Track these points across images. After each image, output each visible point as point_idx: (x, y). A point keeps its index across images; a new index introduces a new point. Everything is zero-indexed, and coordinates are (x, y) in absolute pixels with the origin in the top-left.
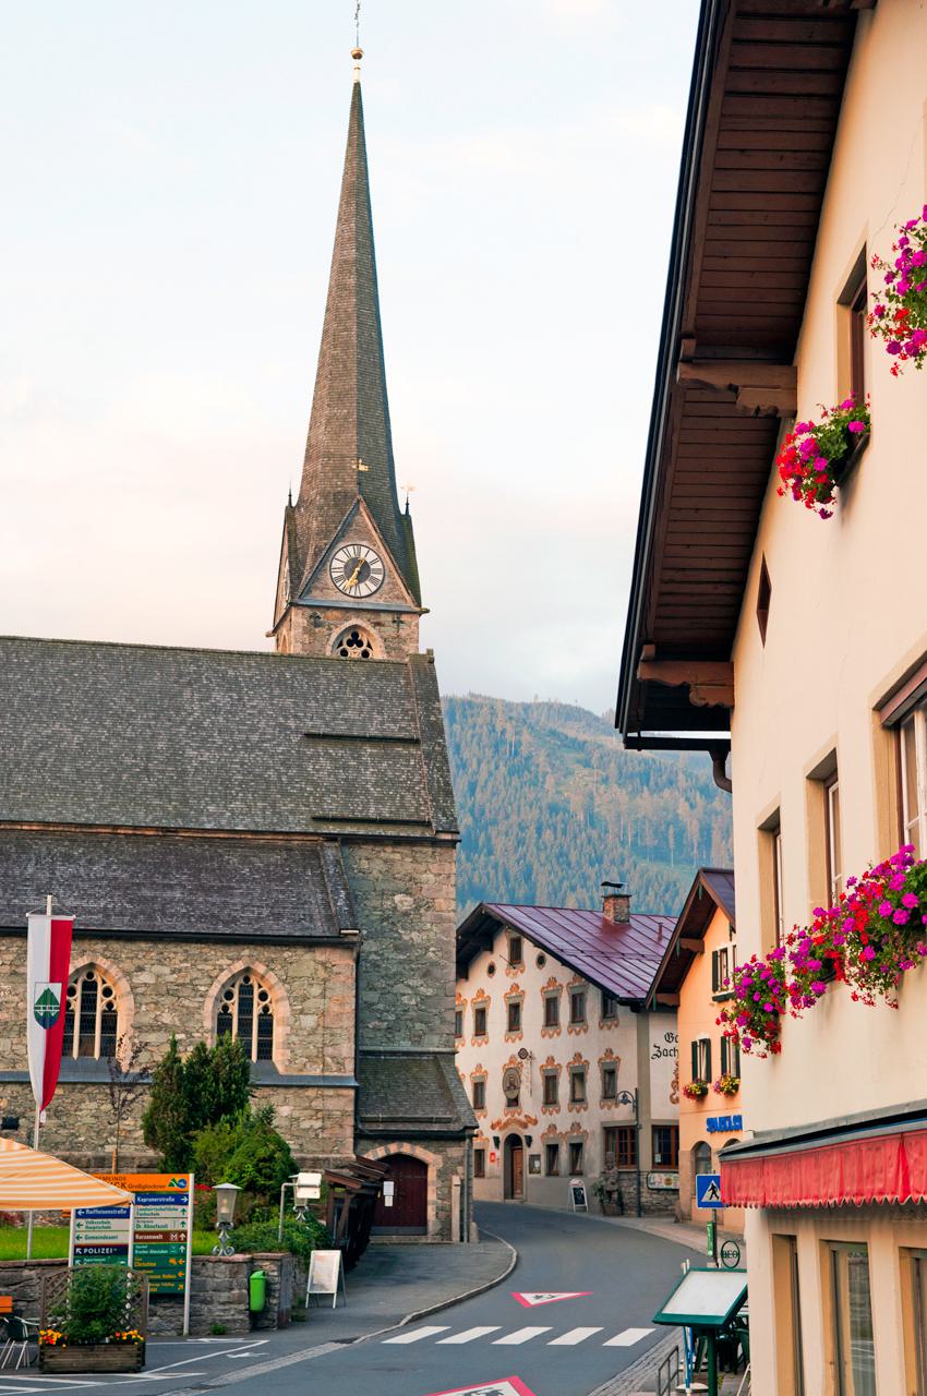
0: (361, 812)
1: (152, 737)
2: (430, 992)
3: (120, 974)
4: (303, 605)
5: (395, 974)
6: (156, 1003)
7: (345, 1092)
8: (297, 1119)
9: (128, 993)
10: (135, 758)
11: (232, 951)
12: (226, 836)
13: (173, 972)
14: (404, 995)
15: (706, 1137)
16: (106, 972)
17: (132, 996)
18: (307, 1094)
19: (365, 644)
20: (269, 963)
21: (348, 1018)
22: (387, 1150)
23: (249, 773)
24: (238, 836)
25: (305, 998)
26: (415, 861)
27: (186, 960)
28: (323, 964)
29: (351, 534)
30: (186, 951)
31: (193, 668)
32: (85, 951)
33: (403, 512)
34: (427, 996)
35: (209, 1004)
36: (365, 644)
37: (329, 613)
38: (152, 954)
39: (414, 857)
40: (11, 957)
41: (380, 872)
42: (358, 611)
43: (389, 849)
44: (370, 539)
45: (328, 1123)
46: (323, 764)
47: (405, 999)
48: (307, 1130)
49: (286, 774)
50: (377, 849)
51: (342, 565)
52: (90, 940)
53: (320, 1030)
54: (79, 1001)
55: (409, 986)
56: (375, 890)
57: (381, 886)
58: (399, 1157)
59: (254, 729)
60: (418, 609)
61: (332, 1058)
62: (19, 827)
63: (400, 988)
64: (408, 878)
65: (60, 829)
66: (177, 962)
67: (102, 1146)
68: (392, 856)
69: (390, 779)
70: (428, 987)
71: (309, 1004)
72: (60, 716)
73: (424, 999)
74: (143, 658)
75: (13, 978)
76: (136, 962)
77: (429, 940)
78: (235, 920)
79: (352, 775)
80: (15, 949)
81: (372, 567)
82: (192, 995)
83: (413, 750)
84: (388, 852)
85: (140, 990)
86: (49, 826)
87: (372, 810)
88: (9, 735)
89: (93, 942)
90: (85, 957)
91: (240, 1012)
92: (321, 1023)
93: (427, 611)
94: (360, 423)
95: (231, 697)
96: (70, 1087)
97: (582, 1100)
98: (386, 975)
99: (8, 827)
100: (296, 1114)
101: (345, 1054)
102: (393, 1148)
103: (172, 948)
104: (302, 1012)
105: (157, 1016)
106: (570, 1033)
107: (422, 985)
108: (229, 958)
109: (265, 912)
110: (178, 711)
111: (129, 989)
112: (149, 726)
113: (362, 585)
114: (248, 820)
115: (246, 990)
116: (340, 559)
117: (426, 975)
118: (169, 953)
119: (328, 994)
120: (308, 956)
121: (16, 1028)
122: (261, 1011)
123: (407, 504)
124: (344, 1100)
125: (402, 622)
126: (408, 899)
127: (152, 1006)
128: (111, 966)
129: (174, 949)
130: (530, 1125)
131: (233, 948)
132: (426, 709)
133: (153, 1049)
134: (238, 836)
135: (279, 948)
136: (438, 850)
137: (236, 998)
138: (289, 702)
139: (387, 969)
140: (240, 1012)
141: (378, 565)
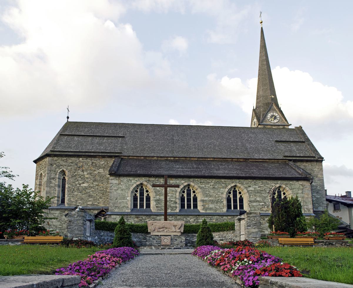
1: (237, 142)
2: (319, 197)
3: (244, 188)
4: (262, 125)
6: (255, 195)
9: (247, 193)
11: (275, 182)
12: (262, 160)
13: (259, 187)
16: (240, 187)
17: (248, 194)
20: (286, 185)
21: (310, 199)
23: (264, 148)
24: (265, 161)
26: (312, 165)
30: (262, 182)
31: (243, 130)
32: (233, 182)
34: (318, 198)
40: (212, 184)
43: (305, 163)
44: (276, 111)
46: (282, 146)
49: (273, 148)
50: (302, 163)
51: (270, 116)
52: (235, 179)
54: (232, 196)
59: (261, 140)
61: (306, 209)
62: (207, 159)
64: (310, 170)
65: (218, 159)
68: (306, 165)
70: (318, 195)
72: (213, 139)
73: (317, 198)
74: (230, 129)
75: (214, 189)
76: (248, 184)
77: (317, 184)
80: (214, 182)
81: (277, 118)
82: (265, 193)
83: (304, 144)
84: (305, 164)
85: (250, 192)
86: (215, 159)
88: (201, 142)
89: (235, 180)
90: (234, 184)
92: (303, 200)
93: (291, 125)
94: (270, 89)
96: (233, 216)
99: (204, 159)
101: (310, 208)
103: (258, 181)
105: (255, 198)
110: (242, 138)
111: (247, 192)
112: (235, 140)
113: (275, 120)
115: (279, 192)
116: (269, 115)
117: (317, 193)
118: (258, 182)
119: (304, 192)
120: (297, 183)
127: (254, 196)
128: (241, 186)
129: (259, 181)
131: (275, 181)
132: (304, 136)
133: (255, 207)
134: (265, 161)
135: (288, 181)
136: (318, 163)
138: (268, 136)
141: (278, 116)
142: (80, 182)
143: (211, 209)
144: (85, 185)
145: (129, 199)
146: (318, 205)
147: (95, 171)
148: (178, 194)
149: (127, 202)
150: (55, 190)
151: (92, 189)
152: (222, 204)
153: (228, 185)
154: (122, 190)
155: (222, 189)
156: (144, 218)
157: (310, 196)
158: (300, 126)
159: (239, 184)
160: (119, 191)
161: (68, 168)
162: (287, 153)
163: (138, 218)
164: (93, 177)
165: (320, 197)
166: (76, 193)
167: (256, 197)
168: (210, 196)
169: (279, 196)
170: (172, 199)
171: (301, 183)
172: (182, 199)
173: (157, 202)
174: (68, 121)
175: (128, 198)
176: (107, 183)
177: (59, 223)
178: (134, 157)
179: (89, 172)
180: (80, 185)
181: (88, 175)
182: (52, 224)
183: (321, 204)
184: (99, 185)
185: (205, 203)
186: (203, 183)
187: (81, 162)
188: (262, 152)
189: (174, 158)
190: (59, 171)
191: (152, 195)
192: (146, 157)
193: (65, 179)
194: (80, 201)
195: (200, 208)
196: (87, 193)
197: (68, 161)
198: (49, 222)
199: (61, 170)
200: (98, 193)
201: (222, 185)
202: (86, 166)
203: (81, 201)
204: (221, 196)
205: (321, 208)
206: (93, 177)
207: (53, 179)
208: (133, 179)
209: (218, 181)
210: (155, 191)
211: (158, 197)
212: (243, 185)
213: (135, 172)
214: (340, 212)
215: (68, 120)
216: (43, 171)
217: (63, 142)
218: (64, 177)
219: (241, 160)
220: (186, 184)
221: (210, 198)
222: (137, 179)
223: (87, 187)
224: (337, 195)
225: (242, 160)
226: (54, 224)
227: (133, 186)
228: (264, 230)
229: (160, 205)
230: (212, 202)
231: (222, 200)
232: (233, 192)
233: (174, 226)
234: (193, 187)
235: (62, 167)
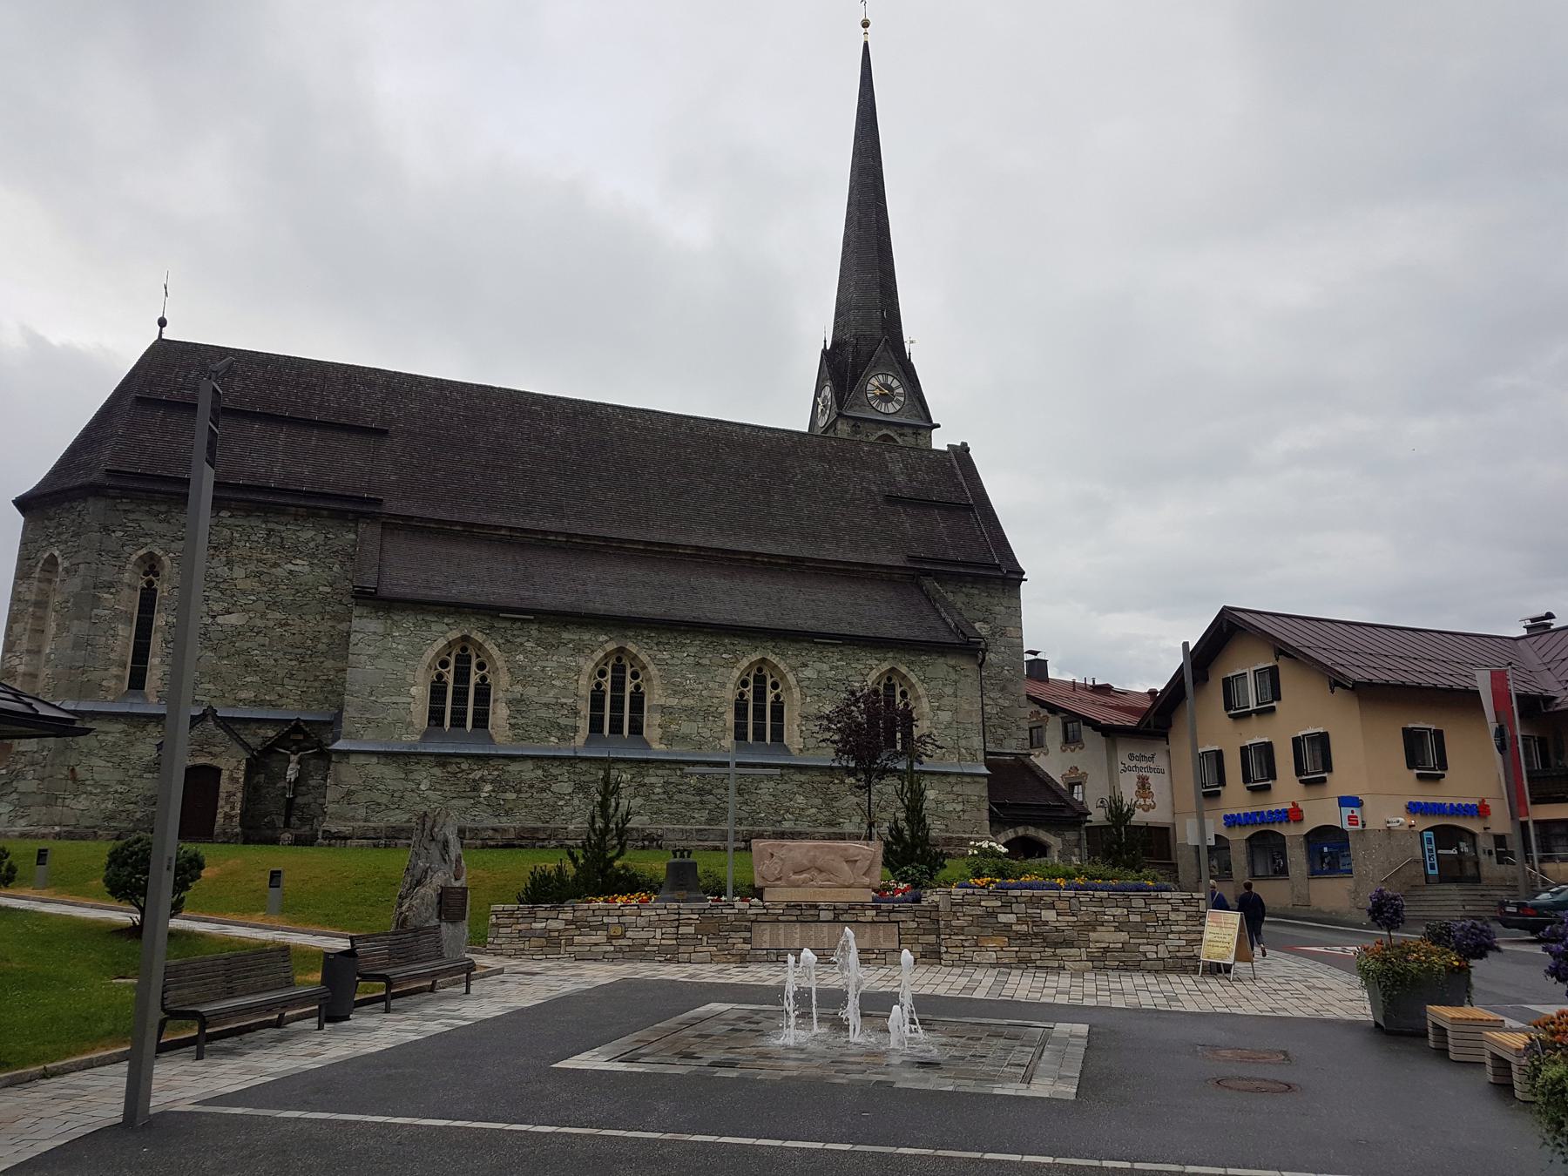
0: (943, 555)
3: (788, 669)
8: (942, 802)
15: (1223, 832)
18: (948, 780)
22: (1016, 832)
25: (940, 697)
27: (841, 659)
32: (757, 647)
34: (1004, 707)
38: (813, 653)
45: (968, 807)
48: (950, 812)
51: (889, 383)
53: (955, 725)
55: (990, 698)
65: (709, 554)
66: (835, 661)
71: (945, 701)
75: (697, 668)
76: (799, 658)
92: (955, 717)
93: (938, 426)
100: (941, 798)
104: (939, 708)
107: (1000, 697)
108: (876, 659)
117: (1003, 689)
118: (829, 652)
119: (959, 694)
120: (941, 660)
121: (702, 713)
124: (979, 787)
125: (919, 434)
127: (816, 698)
143: (685, 738)
144: (234, 619)
145: (420, 692)
146: (1003, 732)
147: (276, 565)
148: (583, 681)
149: (409, 704)
150: (112, 632)
151: (260, 639)
152: (721, 723)
153: (739, 658)
154: (395, 657)
155: (723, 669)
156: (464, 766)
158: (964, 444)
159: (774, 656)
160: (382, 663)
161: (174, 545)
163: (444, 765)
164: (265, 589)
165: (1012, 706)
167: (820, 701)
168: (686, 694)
169: (890, 702)
170: (563, 700)
172: (597, 701)
173: (512, 708)
174: (163, 337)
175: (413, 690)
176: (318, 618)
177: (119, 775)
178: (426, 523)
179: (252, 567)
180: (214, 617)
181: (248, 581)
182: (89, 776)
184: (288, 625)
189: (567, 537)
190: (134, 558)
192: (473, 525)
193: (156, 590)
194: (207, 686)
195: (651, 732)
197: (173, 517)
198: (77, 768)
200: (281, 654)
201: (724, 656)
202: (243, 543)
203: (210, 686)
205: (1014, 743)
206: (265, 589)
207: (109, 588)
208: (436, 619)
210: (510, 666)
211: (518, 688)
214: (1082, 753)
215: (161, 333)
217: (150, 432)
218: (150, 583)
219: (780, 561)
220: (611, 646)
221: (685, 702)
223: (240, 629)
224: (1080, 681)
225: (784, 562)
226: (96, 777)
227: (435, 645)
228: (841, 820)
230: (690, 712)
231: (720, 710)
233: (847, 862)
234: (633, 659)
235: (149, 540)
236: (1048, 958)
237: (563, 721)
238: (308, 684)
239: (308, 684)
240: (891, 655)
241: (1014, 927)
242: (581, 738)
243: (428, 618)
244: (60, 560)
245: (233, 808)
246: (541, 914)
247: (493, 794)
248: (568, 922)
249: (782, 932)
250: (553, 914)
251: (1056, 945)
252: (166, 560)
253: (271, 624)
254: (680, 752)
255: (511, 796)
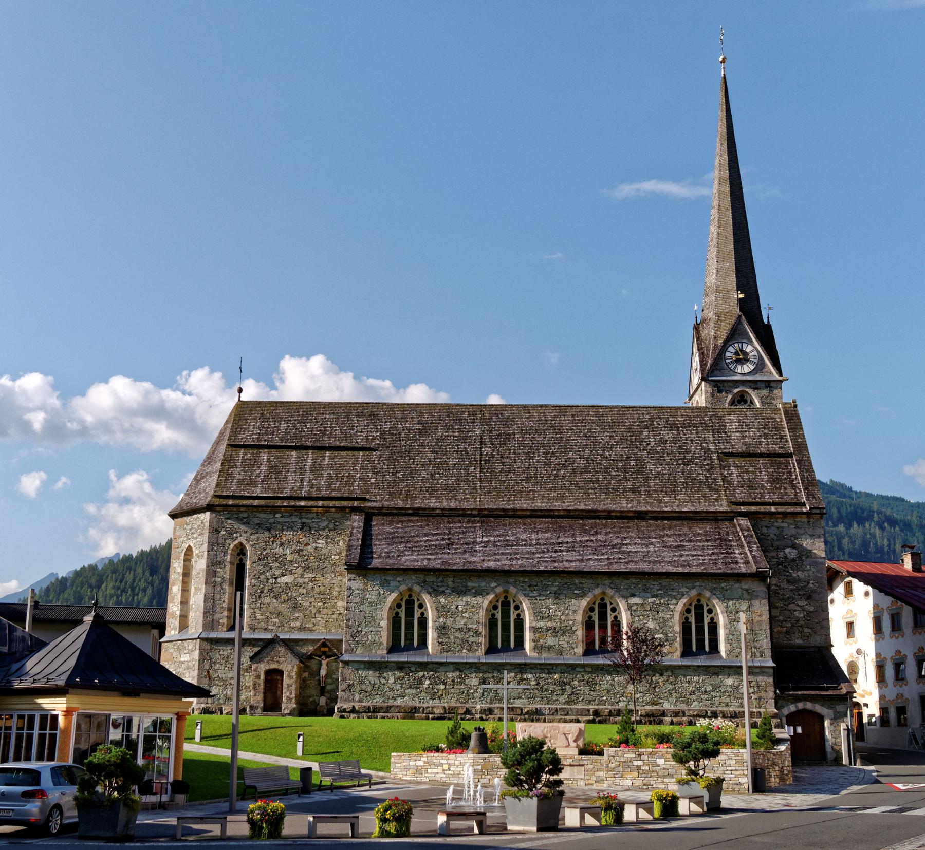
2: (812, 609)
5: (789, 598)
7: (767, 670)
10: (617, 471)
14: (795, 611)
19: (749, 401)
20: (713, 591)
22: (796, 707)
27: (660, 589)
28: (747, 590)
29: (737, 336)
30: (660, 584)
32: (598, 585)
33: (766, 322)
35: (677, 617)
36: (749, 401)
37: (725, 384)
39: (796, 525)
41: (775, 535)
42: (743, 382)
47: (796, 614)
55: (798, 605)
56: (772, 546)
57: (776, 544)
58: (805, 711)
60: (781, 378)
63: (792, 606)
67: (617, 703)
68: (782, 525)
69: (777, 478)
76: (630, 591)
77: (809, 576)
78: (689, 565)
79: (752, 476)
85: (634, 608)
87: (767, 496)
91: (599, 620)
95: (672, 433)
97: (903, 679)
98: (783, 599)
102: (801, 705)
106: (891, 637)
109: (707, 559)
110: (641, 442)
114: (689, 505)
117: (809, 598)
120: (737, 585)
122: (516, 617)
123: (768, 318)
126: (794, 551)
127: (641, 617)
128: (614, 594)
129: (653, 583)
130: (866, 696)
137: (693, 612)
139: (783, 594)
140: (406, 616)
142: (277, 573)
143: (549, 648)
146: (810, 630)
147: (307, 544)
148: (482, 613)
151: (302, 591)
157: (766, 617)
162: (742, 492)
166: (267, 600)
168: (549, 618)
170: (470, 626)
171: (746, 587)
174: (241, 399)
179: (294, 547)
180: (276, 579)
183: (819, 628)
185: (537, 635)
186: (536, 588)
187: (279, 523)
188: (681, 489)
190: (232, 546)
191: (430, 615)
196: (290, 599)
199: (236, 542)
201: (575, 592)
203: (277, 620)
204: (572, 617)
209: (566, 583)
212: (619, 592)
213: (396, 559)
215: (239, 397)
216: (194, 541)
218: (241, 560)
221: (549, 624)
222: (401, 579)
228: (662, 701)
229: (447, 640)
230: (555, 632)
231: (574, 628)
232: (599, 607)
236: (659, 783)
237: (471, 640)
238: (329, 616)
239: (329, 616)
240: (698, 584)
241: (642, 768)
242: (482, 650)
243: (388, 578)
244: (194, 549)
245: (291, 693)
246: (413, 758)
247: (431, 686)
248: (425, 762)
249: (575, 771)
250: (418, 758)
251: (664, 777)
252: (248, 547)
253: (307, 580)
254: (547, 658)
255: (442, 687)
